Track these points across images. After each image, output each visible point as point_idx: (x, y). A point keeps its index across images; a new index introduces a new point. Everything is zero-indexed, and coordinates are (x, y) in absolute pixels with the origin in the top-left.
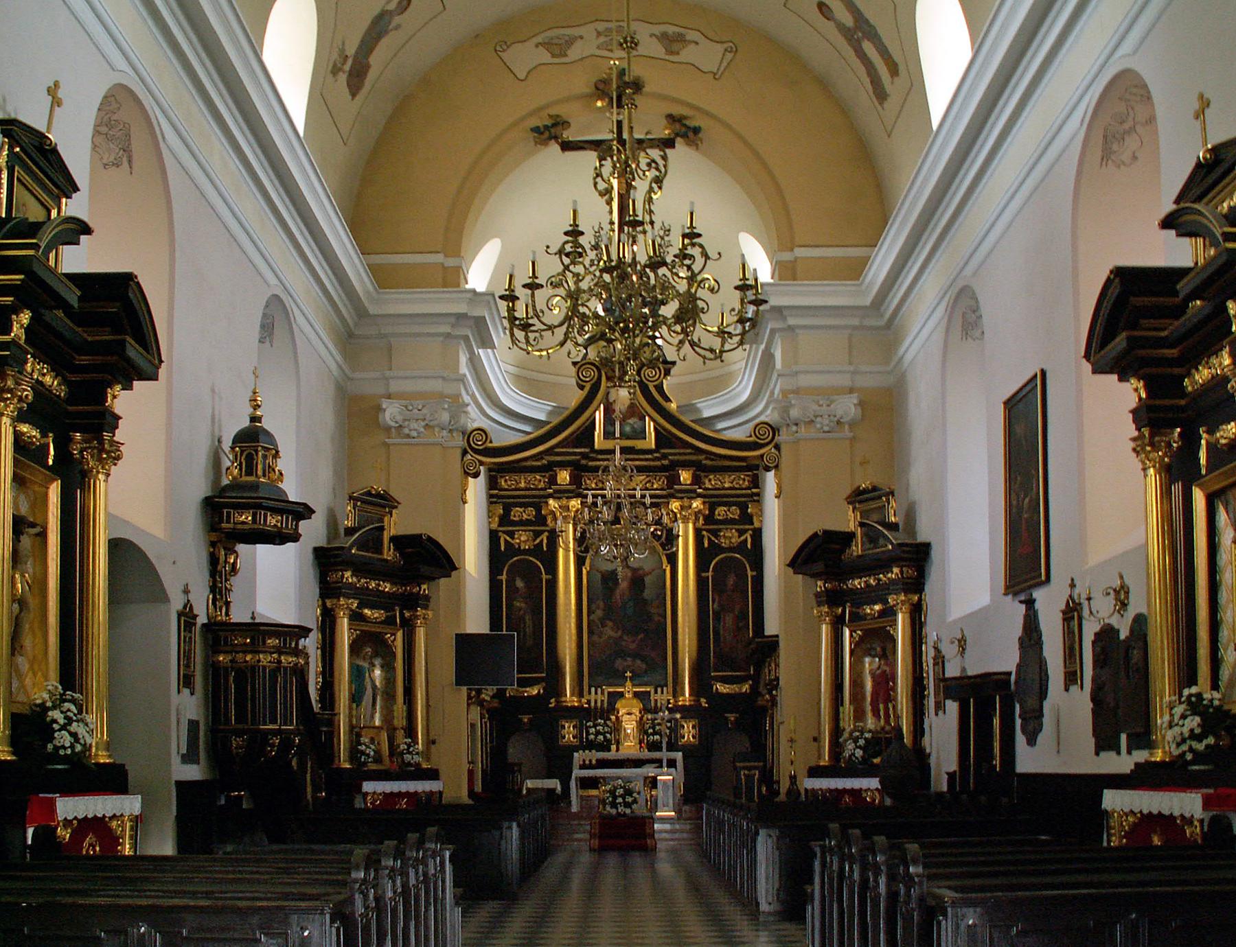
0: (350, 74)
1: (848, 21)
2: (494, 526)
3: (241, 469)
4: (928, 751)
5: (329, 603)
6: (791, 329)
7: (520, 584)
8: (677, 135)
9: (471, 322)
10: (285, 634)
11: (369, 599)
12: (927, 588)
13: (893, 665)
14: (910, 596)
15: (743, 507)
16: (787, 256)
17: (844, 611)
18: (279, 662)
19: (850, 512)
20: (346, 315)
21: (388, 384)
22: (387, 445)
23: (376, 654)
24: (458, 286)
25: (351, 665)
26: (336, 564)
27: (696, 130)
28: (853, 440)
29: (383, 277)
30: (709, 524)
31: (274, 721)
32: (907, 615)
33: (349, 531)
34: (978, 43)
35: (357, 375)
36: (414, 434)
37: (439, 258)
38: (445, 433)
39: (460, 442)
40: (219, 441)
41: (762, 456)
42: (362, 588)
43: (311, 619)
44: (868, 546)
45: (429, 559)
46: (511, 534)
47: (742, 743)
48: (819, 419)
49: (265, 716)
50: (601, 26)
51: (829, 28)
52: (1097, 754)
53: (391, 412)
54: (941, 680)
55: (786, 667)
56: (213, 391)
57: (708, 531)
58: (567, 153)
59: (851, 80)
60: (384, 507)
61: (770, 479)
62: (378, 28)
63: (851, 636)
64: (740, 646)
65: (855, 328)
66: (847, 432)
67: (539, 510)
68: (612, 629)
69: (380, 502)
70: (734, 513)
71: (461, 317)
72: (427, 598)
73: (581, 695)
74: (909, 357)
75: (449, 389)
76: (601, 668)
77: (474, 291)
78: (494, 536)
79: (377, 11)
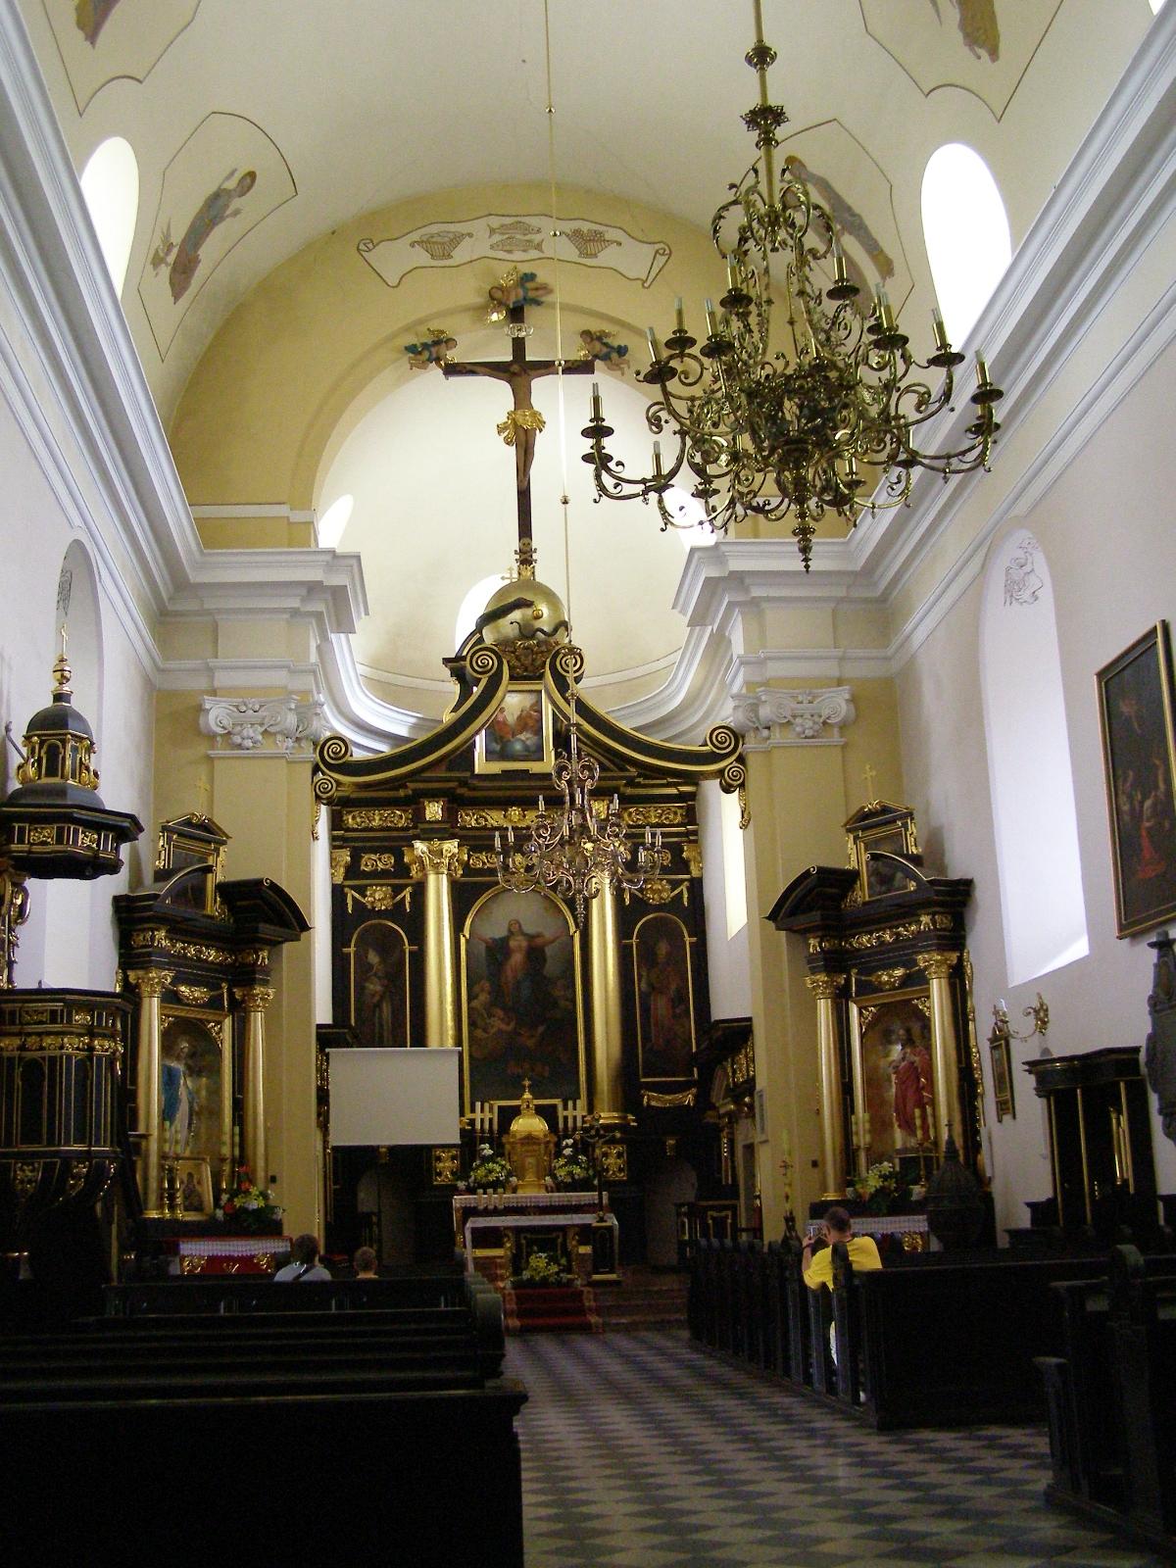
0: (174, 270)
4: (988, 1174)
6: (755, 602)
7: (373, 958)
8: (596, 357)
14: (947, 955)
17: (848, 981)
18: (91, 1049)
19: (851, 844)
21: (212, 678)
22: (210, 759)
26: (148, 920)
27: (622, 351)
28: (844, 747)
29: (210, 534)
32: (944, 982)
33: (161, 875)
35: (174, 664)
36: (248, 743)
37: (283, 511)
38: (290, 742)
39: (311, 755)
40: (8, 729)
44: (878, 888)
46: (362, 890)
48: (798, 720)
49: (68, 1133)
50: (495, 222)
52: (1029, 1205)
53: (217, 715)
55: (764, 1062)
58: (451, 379)
62: (214, 210)
63: (861, 1014)
65: (840, 600)
66: (836, 737)
67: (399, 856)
68: (502, 1020)
71: (313, 588)
72: (266, 971)
74: (919, 637)
77: (332, 552)
79: (212, 189)
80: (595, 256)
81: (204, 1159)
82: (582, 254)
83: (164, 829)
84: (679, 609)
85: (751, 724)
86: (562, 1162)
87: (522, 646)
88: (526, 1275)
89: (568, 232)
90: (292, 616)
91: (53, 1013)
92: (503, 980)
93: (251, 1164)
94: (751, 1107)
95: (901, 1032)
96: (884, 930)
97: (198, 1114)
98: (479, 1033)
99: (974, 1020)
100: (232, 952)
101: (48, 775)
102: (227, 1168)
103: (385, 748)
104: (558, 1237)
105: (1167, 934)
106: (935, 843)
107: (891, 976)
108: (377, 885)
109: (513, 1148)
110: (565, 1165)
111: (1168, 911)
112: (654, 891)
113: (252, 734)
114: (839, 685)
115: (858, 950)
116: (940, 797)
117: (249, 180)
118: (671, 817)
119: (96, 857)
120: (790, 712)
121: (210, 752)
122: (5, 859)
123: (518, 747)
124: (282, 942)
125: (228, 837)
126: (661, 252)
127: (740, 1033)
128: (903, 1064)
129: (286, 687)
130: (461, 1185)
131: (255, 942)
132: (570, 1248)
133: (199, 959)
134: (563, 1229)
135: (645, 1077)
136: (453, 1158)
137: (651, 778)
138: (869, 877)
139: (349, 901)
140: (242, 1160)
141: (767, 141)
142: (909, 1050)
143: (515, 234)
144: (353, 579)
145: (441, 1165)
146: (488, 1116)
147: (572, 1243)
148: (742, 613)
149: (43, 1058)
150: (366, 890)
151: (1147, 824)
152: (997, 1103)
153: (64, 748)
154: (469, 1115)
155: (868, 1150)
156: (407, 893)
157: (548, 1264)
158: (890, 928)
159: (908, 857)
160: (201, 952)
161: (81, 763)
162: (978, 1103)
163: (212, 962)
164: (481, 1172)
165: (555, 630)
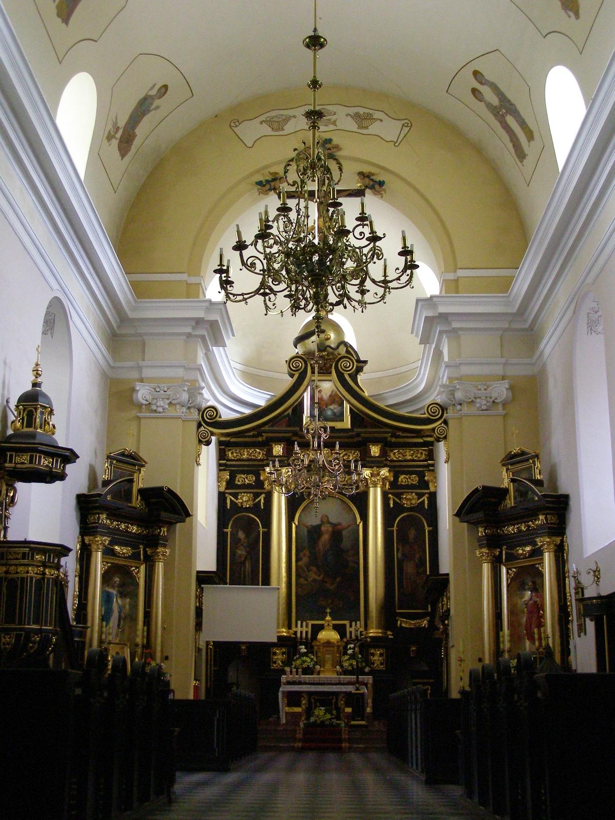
0: (121, 141)
1: (495, 101)
5: (87, 539)
6: (455, 331)
7: (241, 535)
8: (367, 187)
9: (208, 326)
10: (50, 551)
12: (568, 532)
13: (542, 598)
14: (554, 538)
15: (421, 475)
16: (451, 276)
17: (501, 553)
18: (44, 574)
19: (504, 473)
20: (110, 317)
21: (141, 372)
22: (139, 418)
24: (198, 297)
25: (103, 592)
26: (96, 508)
27: (381, 184)
28: (505, 416)
29: (140, 290)
30: (393, 490)
32: (552, 554)
33: (106, 483)
34: (591, 102)
35: (118, 364)
36: (160, 409)
37: (184, 277)
38: (184, 409)
39: (196, 416)
40: (7, 402)
41: (433, 429)
42: (115, 529)
43: (72, 540)
45: (168, 508)
46: (235, 495)
48: (478, 400)
49: (29, 618)
53: (143, 393)
54: (581, 600)
56: (5, 363)
59: (498, 145)
60: (134, 465)
61: (442, 449)
62: (143, 107)
63: (508, 573)
64: (419, 586)
65: (505, 330)
66: (500, 410)
67: (258, 475)
68: (315, 573)
70: (414, 480)
71: (198, 322)
73: (290, 627)
75: (191, 375)
77: (210, 301)
78: (222, 497)
79: (142, 96)
80: (367, 128)
81: (126, 645)
82: (359, 127)
84: (414, 334)
85: (450, 402)
86: (347, 657)
88: (312, 719)
89: (352, 114)
90: (187, 337)
91: (24, 554)
92: (317, 549)
93: (153, 649)
95: (530, 583)
97: (123, 619)
98: (302, 581)
100: (146, 528)
101: (27, 427)
102: (139, 650)
103: (247, 411)
104: (333, 699)
107: (523, 550)
108: (244, 493)
109: (319, 648)
110: (348, 660)
112: (407, 499)
113: (162, 404)
114: (503, 380)
115: (506, 535)
117: (163, 90)
118: (419, 455)
119: (51, 471)
120: (473, 395)
121: (138, 414)
122: (2, 471)
123: (329, 413)
124: (176, 523)
125: (146, 462)
126: (406, 125)
128: (530, 602)
129: (183, 378)
130: (287, 669)
131: (160, 523)
132: (339, 705)
133: (127, 531)
134: (336, 694)
135: (399, 609)
136: (283, 653)
138: (514, 492)
139: (228, 502)
140: (148, 645)
141: (314, 127)
142: (534, 594)
144: (222, 314)
145: (276, 657)
146: (304, 629)
147: (342, 703)
148: (448, 338)
149: (18, 578)
150: (238, 495)
152: (578, 625)
153: (36, 412)
154: (294, 629)
155: (509, 652)
156: (262, 497)
157: (325, 714)
158: (525, 522)
160: (128, 527)
161: (45, 420)
162: (570, 626)
163: (135, 533)
164: (299, 662)
165: (338, 346)
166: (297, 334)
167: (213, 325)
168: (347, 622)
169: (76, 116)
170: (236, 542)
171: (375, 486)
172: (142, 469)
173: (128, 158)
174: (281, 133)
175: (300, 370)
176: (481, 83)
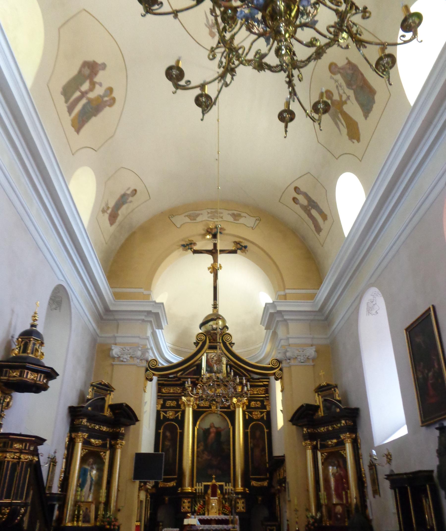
2: (159, 408)
3: (20, 350)
7: (168, 434)
8: (238, 249)
11: (93, 434)
15: (262, 402)
16: (282, 293)
17: (317, 443)
18: (20, 458)
22: (112, 365)
23: (94, 463)
27: (245, 247)
29: (117, 296)
30: (248, 409)
31: (8, 497)
36: (125, 360)
37: (142, 290)
38: (139, 361)
39: (145, 364)
45: (125, 416)
46: (165, 412)
47: (265, 513)
48: (299, 357)
50: (209, 211)
51: (297, 208)
53: (116, 351)
55: (291, 471)
57: (248, 412)
60: (107, 390)
62: (123, 200)
63: (322, 455)
65: (312, 320)
66: (311, 363)
67: (177, 401)
69: (106, 388)
71: (149, 313)
72: (123, 435)
76: (202, 472)
78: (158, 413)
79: (123, 192)
80: (238, 220)
83: (92, 385)
87: (213, 335)
94: (285, 487)
96: (329, 426)
99: (362, 459)
105: (443, 424)
106: (345, 396)
107: (332, 442)
111: (444, 415)
116: (346, 380)
117: (134, 192)
127: (281, 461)
137: (254, 378)
143: (214, 214)
146: (200, 487)
151: (431, 382)
158: (331, 425)
159: (336, 400)
160: (100, 427)
165: (223, 328)
166: (201, 321)
167: (157, 315)
168: (223, 483)
169: (83, 193)
170: (165, 437)
171: (239, 406)
172: (112, 393)
173: (114, 226)
174: (194, 221)
175: (200, 345)
176: (298, 194)
